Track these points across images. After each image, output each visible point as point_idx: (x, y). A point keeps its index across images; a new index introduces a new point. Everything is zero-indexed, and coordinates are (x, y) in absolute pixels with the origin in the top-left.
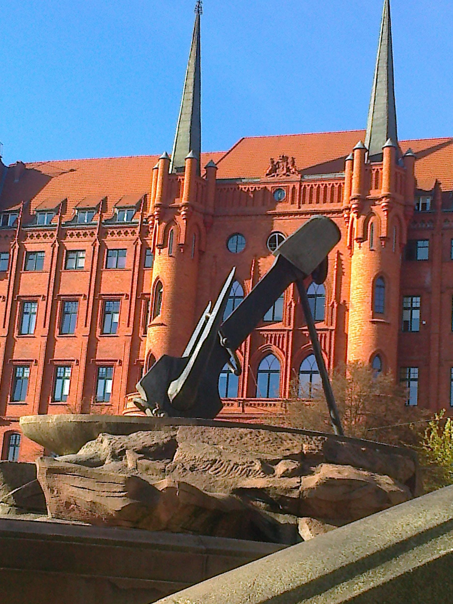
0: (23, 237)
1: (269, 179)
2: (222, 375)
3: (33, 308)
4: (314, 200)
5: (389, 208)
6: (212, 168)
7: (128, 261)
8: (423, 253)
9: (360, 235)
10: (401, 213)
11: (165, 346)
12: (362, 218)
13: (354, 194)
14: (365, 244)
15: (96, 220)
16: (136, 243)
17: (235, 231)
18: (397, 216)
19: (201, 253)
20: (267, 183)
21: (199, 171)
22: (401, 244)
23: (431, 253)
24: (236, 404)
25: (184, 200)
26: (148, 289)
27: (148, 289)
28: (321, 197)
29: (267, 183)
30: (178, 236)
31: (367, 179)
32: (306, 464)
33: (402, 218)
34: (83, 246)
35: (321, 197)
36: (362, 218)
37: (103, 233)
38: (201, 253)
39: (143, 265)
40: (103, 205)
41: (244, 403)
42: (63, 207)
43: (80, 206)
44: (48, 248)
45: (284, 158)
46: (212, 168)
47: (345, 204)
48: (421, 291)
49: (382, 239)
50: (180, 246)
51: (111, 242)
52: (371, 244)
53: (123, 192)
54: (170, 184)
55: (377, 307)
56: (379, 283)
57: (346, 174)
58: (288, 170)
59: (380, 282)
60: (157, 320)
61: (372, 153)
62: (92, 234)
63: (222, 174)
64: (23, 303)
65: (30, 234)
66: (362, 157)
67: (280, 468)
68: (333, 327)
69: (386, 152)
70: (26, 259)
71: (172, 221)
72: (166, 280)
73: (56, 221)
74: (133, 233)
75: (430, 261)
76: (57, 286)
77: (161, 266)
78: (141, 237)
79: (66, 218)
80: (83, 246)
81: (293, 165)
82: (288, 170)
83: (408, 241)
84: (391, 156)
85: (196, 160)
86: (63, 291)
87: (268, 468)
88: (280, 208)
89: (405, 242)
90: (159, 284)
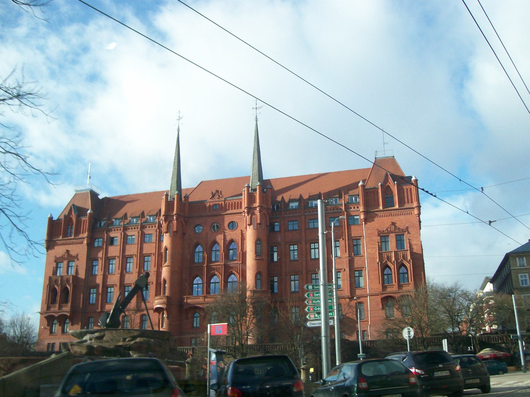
0: (110, 230)
1: (211, 200)
2: (194, 286)
3: (114, 262)
4: (230, 208)
5: (260, 211)
6: (187, 197)
7: (154, 239)
8: (277, 229)
9: (249, 223)
10: (266, 213)
11: (45, 291)
12: (250, 215)
13: (246, 206)
14: (252, 226)
15: (139, 222)
16: (156, 231)
17: (198, 224)
18: (264, 214)
19: (184, 234)
20: (211, 202)
21: (181, 199)
22: (267, 225)
23: (280, 228)
24: (201, 297)
25: (175, 212)
26: (163, 250)
27: (163, 250)
28: (233, 207)
29: (211, 202)
30: (173, 227)
31: (251, 198)
32: (134, 338)
33: (267, 214)
34: (134, 234)
35: (233, 207)
36: (250, 215)
37: (143, 227)
38: (184, 234)
39: (160, 241)
40: (143, 215)
41: (205, 297)
42: (125, 216)
43: (150, 214)
44: (136, 233)
45: (217, 191)
46: (187, 197)
47: (243, 209)
48: (278, 244)
49: (258, 224)
50: (174, 232)
51: (129, 233)
52: (254, 227)
53: (149, 208)
54: (169, 205)
55: (257, 254)
56: (258, 242)
57: (243, 197)
58: (219, 196)
59: (259, 242)
60: (167, 264)
61: (253, 188)
62: (138, 228)
63: (190, 200)
64: (109, 260)
65: (130, 228)
66: (248, 190)
67: (127, 340)
68: (241, 262)
69: (258, 188)
70: (111, 241)
71: (253, 214)
72: (169, 247)
73: (122, 224)
74: (155, 226)
75: (280, 231)
76: (141, 249)
77: (166, 241)
78: (141, 229)
79: (126, 222)
80: (134, 234)
81: (221, 194)
82: (219, 196)
83: (270, 224)
84: (260, 189)
85: (179, 195)
86: (109, 255)
87: (124, 340)
88: (228, 212)
89: (268, 224)
90: (166, 249)
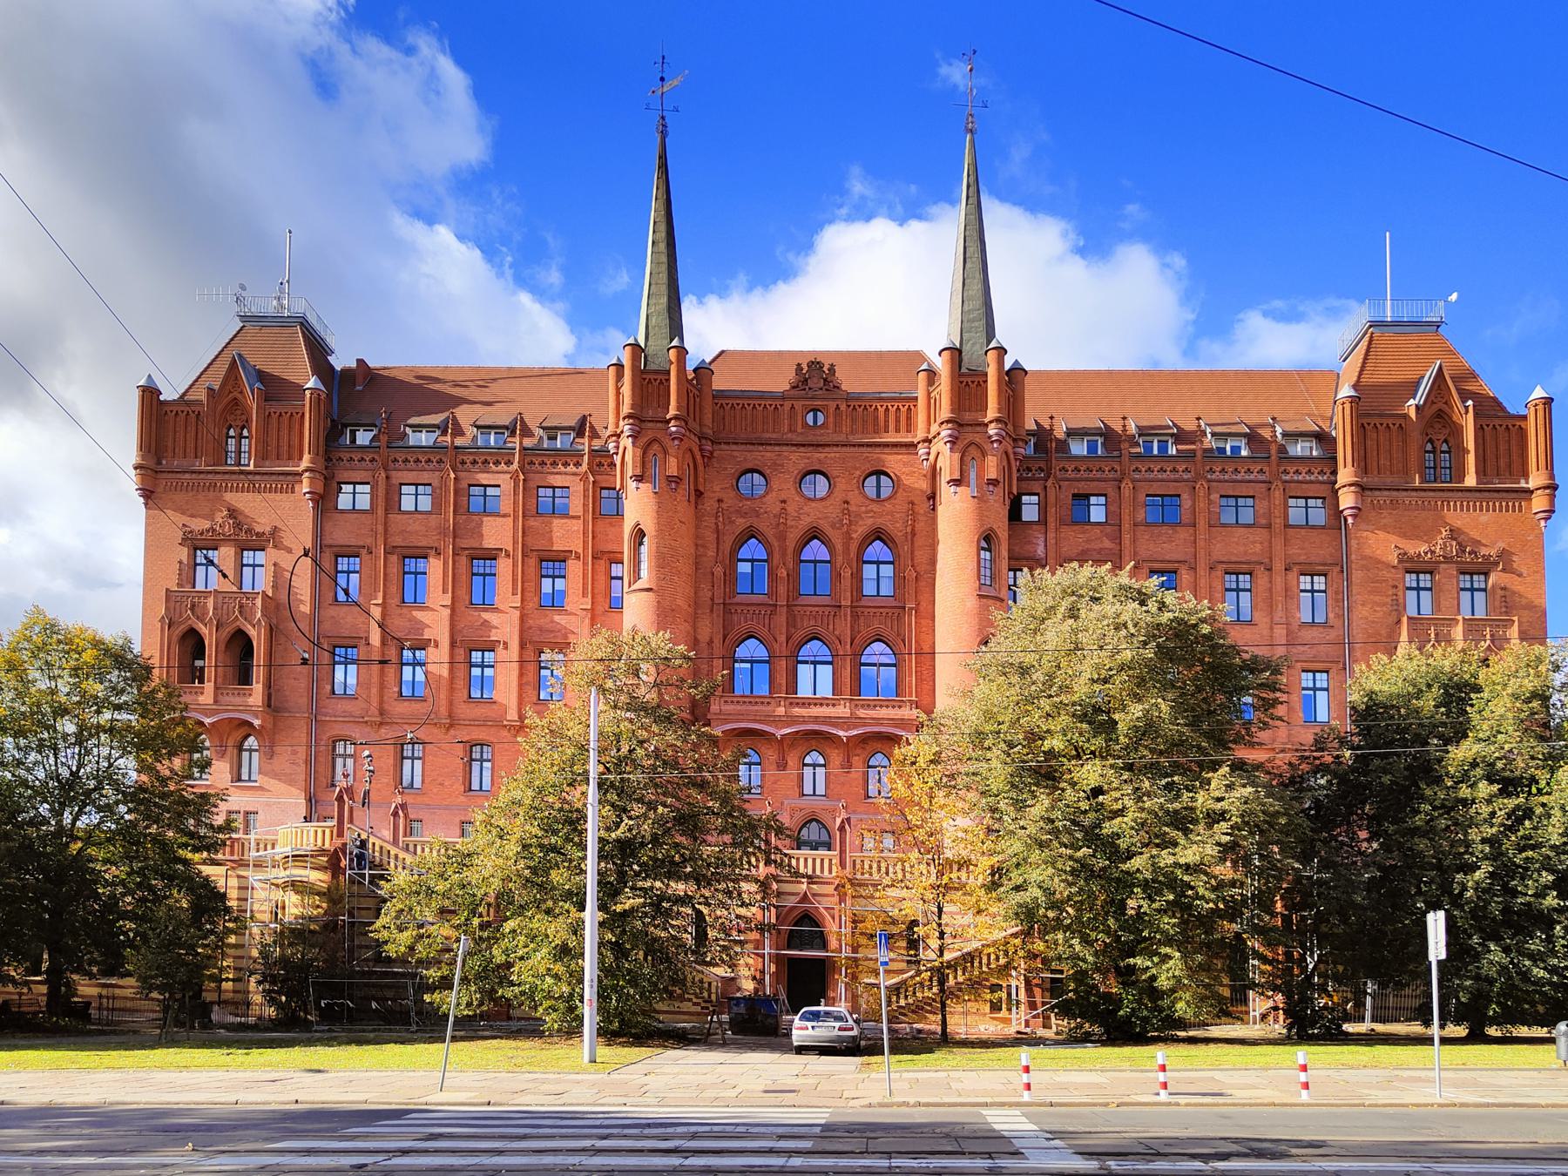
17: (749, 466)
19: (699, 494)
